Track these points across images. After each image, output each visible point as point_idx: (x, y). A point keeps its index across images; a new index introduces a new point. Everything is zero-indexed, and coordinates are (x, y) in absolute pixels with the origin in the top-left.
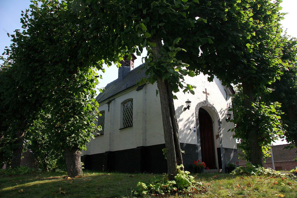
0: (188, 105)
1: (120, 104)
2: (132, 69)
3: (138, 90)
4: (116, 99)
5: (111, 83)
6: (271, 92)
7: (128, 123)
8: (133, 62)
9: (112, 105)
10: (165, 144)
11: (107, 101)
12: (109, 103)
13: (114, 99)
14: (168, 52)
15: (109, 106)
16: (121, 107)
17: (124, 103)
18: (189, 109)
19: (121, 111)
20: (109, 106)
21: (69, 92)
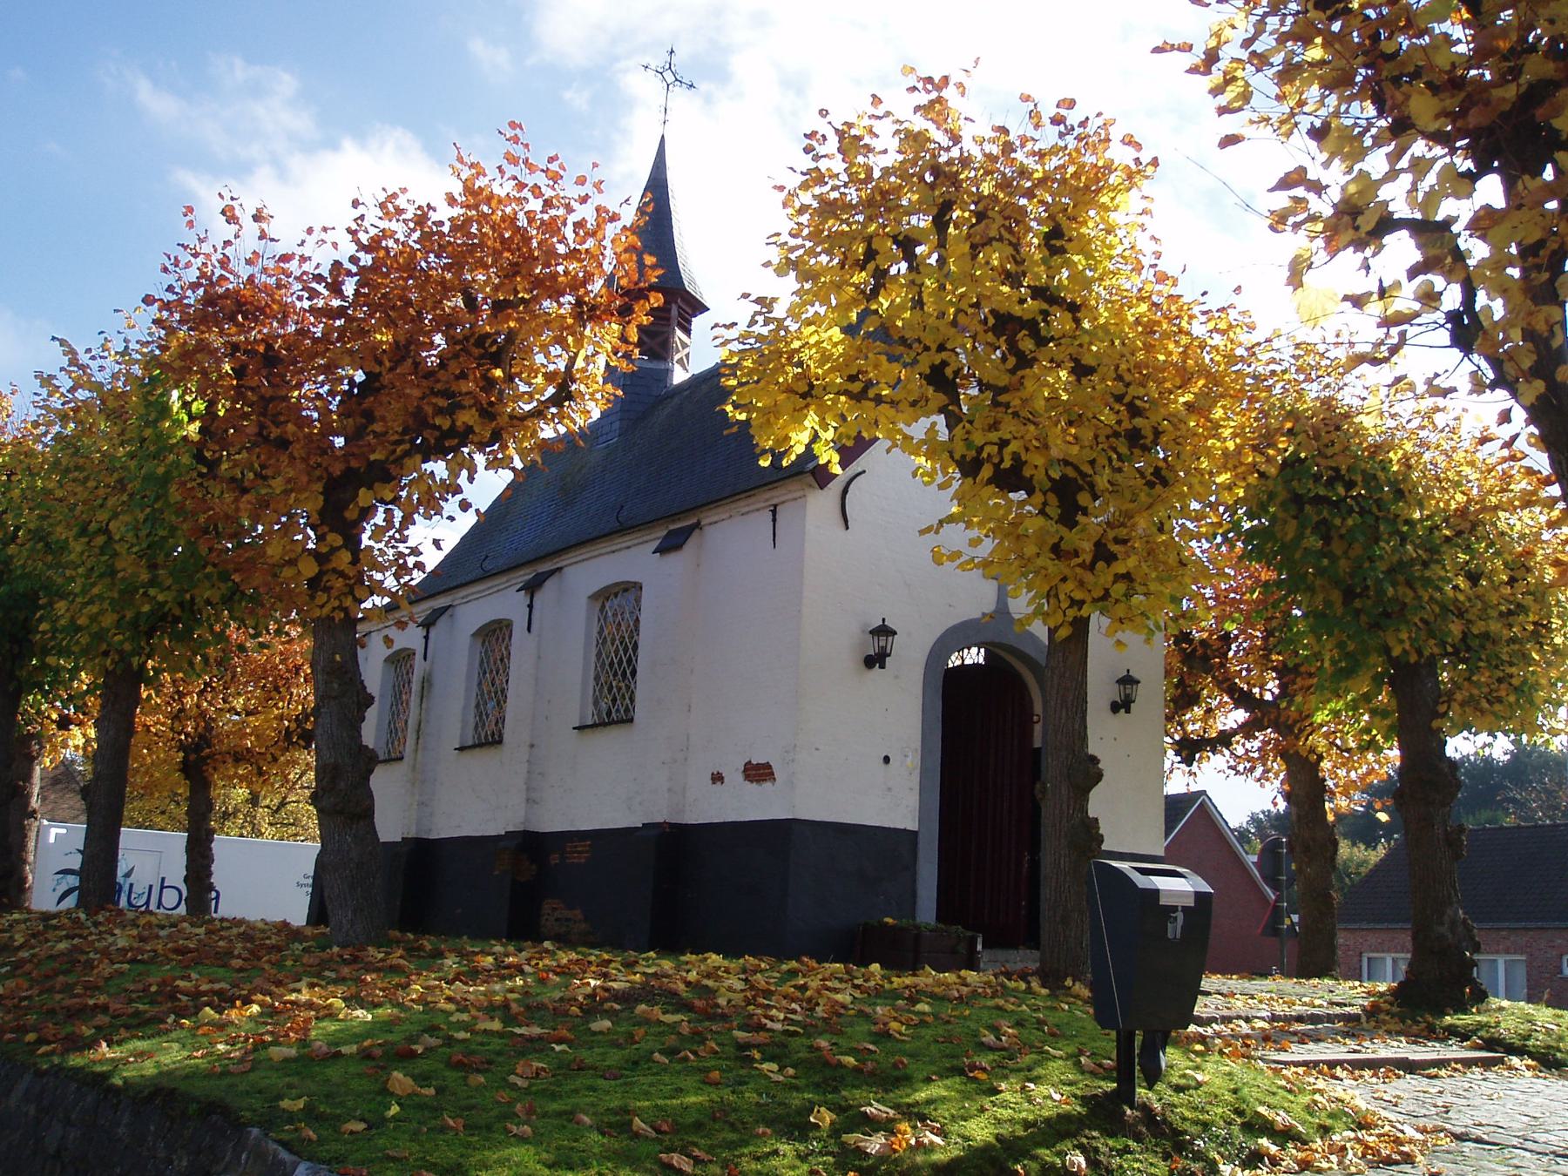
0: (1127, 696)
1: (584, 600)
2: (679, 376)
3: (662, 550)
4: (570, 572)
5: (507, 488)
6: (1208, 983)
7: (614, 701)
8: (688, 332)
9: (544, 596)
10: (915, 833)
11: (526, 575)
12: (532, 588)
13: (560, 569)
14: (377, 485)
15: (531, 606)
16: (588, 619)
17: (604, 596)
18: (1128, 711)
19: (588, 636)
20: (531, 606)
21: (1473, 72)
